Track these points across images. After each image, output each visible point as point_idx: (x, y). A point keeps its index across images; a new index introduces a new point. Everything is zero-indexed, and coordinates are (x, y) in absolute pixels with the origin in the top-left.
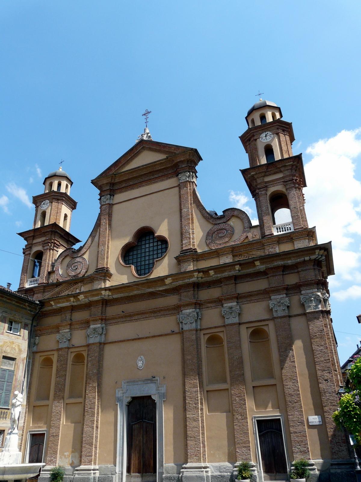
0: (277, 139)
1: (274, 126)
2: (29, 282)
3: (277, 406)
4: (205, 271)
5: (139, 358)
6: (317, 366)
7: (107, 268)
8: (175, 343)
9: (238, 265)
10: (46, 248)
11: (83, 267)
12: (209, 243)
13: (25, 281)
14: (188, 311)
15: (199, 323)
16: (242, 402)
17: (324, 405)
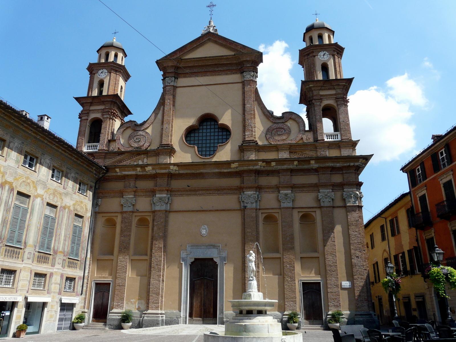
0: (332, 60)
1: (331, 48)
2: (86, 146)
3: (318, 273)
4: (268, 162)
5: (203, 227)
6: (351, 246)
7: (172, 145)
8: (236, 219)
9: (297, 161)
10: (105, 116)
11: (146, 141)
12: (269, 138)
13: (83, 145)
14: (250, 193)
15: (258, 204)
16: (292, 268)
17: (354, 274)
